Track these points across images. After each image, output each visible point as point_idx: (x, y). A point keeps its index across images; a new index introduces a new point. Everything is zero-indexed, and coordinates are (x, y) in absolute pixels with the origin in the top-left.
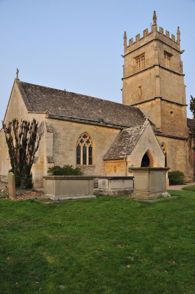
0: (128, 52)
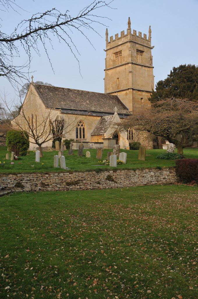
0: (109, 48)
